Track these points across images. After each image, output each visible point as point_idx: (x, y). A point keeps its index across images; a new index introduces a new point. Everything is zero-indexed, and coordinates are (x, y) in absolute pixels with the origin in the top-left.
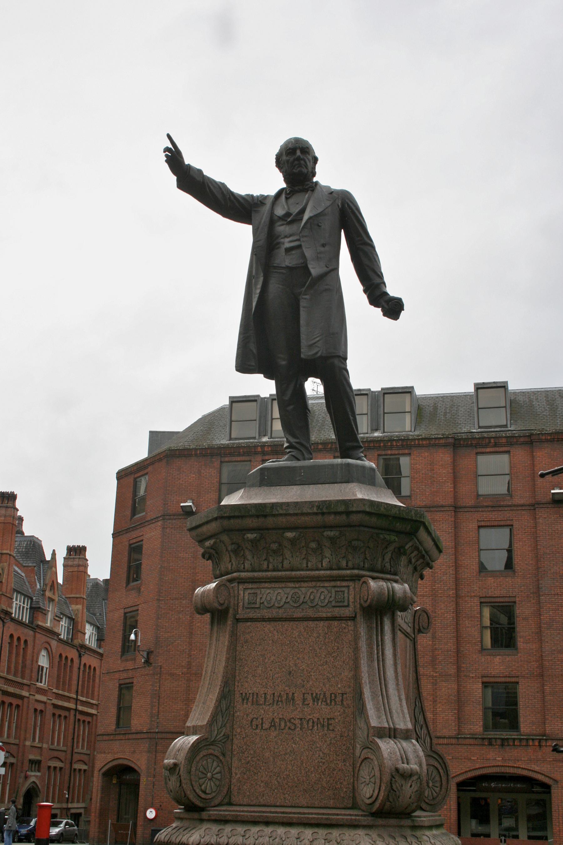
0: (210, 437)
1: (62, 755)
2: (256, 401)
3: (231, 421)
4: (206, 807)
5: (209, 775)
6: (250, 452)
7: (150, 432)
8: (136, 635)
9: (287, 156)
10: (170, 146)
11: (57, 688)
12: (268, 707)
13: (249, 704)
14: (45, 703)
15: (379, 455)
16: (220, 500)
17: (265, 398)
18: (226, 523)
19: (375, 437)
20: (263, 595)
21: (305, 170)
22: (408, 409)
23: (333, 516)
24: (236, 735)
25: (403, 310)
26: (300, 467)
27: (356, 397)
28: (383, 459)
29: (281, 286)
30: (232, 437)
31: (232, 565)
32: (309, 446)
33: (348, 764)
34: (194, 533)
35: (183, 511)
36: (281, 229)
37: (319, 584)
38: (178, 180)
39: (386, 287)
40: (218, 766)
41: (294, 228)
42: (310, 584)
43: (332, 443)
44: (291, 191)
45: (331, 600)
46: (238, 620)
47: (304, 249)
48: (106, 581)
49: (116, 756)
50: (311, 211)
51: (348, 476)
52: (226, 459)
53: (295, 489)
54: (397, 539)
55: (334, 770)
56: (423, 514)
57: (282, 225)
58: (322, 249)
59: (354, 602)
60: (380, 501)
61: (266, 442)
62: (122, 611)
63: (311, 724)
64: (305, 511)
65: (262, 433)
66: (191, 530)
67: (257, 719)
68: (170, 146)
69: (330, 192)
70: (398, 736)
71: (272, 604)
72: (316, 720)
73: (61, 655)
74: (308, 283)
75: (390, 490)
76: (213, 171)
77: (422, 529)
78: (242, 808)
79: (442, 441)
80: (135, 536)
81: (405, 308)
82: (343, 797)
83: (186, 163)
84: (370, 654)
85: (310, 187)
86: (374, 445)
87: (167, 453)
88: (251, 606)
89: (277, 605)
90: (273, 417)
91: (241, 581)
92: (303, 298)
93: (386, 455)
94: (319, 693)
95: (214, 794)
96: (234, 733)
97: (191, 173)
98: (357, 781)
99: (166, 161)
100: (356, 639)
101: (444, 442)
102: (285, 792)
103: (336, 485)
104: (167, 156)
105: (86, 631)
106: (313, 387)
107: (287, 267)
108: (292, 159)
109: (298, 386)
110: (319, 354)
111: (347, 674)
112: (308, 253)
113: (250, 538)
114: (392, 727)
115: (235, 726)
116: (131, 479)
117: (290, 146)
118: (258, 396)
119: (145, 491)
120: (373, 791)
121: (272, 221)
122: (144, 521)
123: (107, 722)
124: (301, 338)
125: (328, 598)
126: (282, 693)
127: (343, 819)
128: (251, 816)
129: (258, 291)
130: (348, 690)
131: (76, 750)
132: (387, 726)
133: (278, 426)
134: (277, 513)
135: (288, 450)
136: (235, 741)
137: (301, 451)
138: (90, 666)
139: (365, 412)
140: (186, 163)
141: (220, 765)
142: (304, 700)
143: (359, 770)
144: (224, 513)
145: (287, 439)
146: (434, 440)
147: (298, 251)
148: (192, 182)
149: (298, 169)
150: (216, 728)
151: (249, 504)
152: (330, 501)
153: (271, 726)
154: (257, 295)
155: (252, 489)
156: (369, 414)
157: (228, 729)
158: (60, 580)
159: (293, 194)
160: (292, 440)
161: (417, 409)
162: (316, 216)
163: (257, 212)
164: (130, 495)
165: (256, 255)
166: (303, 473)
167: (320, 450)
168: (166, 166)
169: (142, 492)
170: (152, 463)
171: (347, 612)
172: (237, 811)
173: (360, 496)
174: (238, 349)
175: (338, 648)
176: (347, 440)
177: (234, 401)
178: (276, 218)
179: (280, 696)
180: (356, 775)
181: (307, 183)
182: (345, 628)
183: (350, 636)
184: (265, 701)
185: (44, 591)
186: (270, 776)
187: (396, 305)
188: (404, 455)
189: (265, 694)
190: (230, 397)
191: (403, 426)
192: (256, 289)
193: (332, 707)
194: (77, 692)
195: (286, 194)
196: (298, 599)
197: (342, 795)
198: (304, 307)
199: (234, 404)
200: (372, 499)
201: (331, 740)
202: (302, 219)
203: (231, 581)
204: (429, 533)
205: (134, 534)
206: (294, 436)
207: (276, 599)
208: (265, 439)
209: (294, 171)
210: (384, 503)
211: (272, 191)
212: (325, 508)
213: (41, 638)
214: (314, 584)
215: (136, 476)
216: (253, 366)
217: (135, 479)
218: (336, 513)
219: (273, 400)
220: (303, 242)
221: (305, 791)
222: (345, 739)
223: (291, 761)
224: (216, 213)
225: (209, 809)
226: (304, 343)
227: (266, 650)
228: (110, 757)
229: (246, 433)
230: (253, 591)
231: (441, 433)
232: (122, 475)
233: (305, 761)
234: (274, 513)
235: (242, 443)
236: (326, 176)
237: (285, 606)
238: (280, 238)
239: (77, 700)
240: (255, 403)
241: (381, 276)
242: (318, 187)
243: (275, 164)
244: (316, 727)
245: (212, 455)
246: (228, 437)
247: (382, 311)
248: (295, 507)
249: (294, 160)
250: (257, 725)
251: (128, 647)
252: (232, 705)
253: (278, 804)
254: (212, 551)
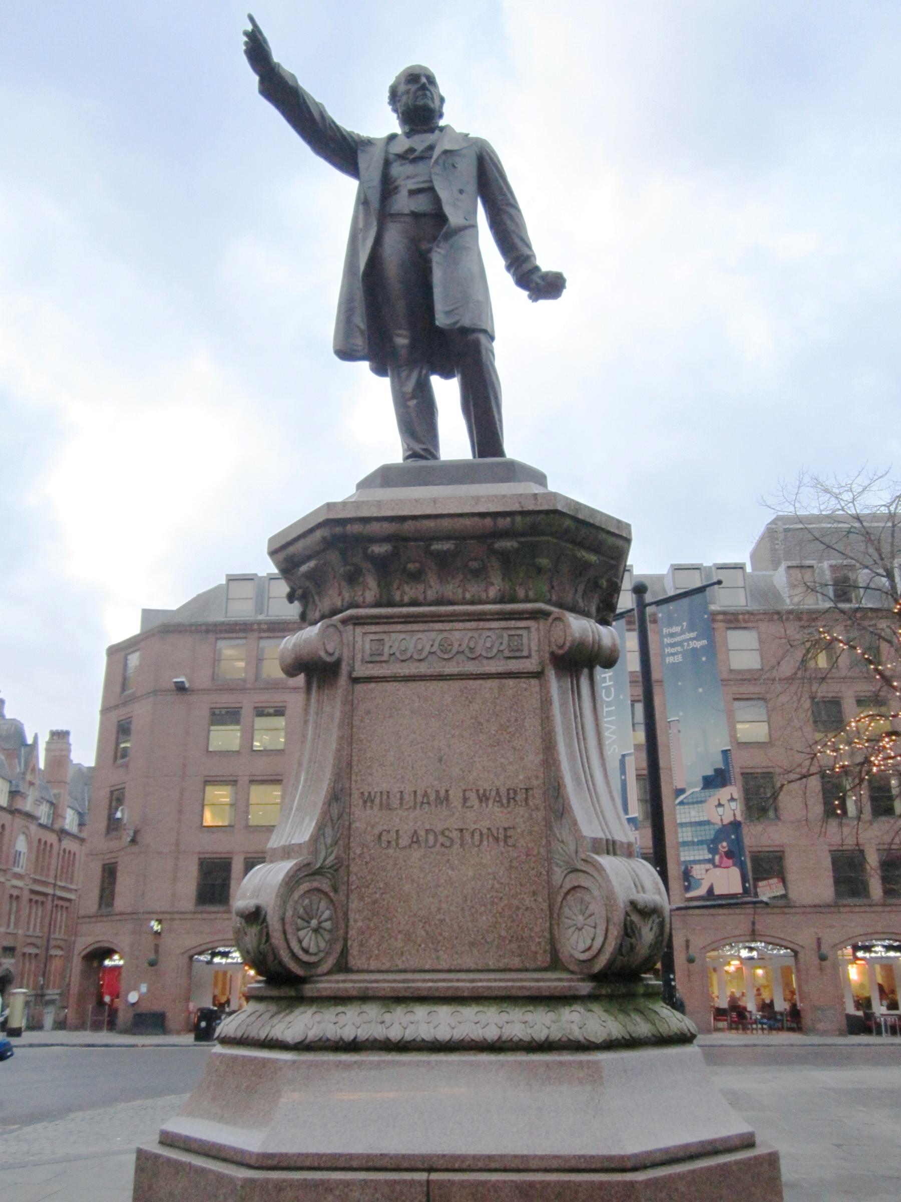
1: (38, 942)
4: (312, 976)
5: (314, 923)
8: (122, 811)
11: (35, 873)
12: (406, 813)
13: (376, 809)
14: (21, 888)
20: (394, 642)
24: (354, 859)
31: (343, 600)
33: (540, 900)
36: (397, 170)
37: (482, 624)
38: (262, 82)
40: (327, 909)
42: (469, 625)
45: (501, 648)
46: (355, 680)
48: (90, 768)
49: (98, 939)
52: (222, 636)
55: (518, 908)
59: (539, 651)
62: (108, 790)
63: (477, 837)
67: (389, 832)
70: (618, 852)
71: (409, 655)
72: (485, 831)
73: (40, 840)
78: (373, 977)
82: (536, 953)
84: (567, 728)
88: (374, 659)
89: (416, 657)
91: (357, 621)
94: (488, 789)
95: (322, 955)
96: (352, 855)
98: (558, 924)
100: (546, 702)
102: (439, 948)
105: (67, 816)
111: (533, 759)
112: (443, 194)
114: (610, 838)
115: (352, 845)
118: (256, 575)
120: (593, 940)
121: (387, 164)
123: (90, 902)
125: (497, 645)
126: (429, 790)
127: (549, 987)
128: (393, 987)
130: (535, 783)
131: (52, 936)
132: (603, 837)
136: (353, 868)
138: (70, 852)
141: (331, 907)
142: (465, 799)
143: (561, 907)
150: (323, 847)
153: (413, 842)
157: (342, 849)
158: (42, 765)
170: (145, 639)
171: (530, 665)
172: (365, 981)
175: (516, 720)
178: (391, 157)
179: (426, 794)
180: (555, 916)
182: (526, 690)
183: (534, 701)
184: (401, 804)
185: (24, 774)
186: (413, 923)
189: (401, 792)
190: (227, 575)
193: (510, 809)
194: (56, 877)
196: (449, 648)
197: (533, 948)
199: (232, 583)
201: (511, 861)
202: (431, 158)
203: (344, 622)
207: (415, 647)
213: (19, 821)
214: (473, 624)
221: (472, 944)
222: (534, 859)
223: (447, 897)
225: (315, 978)
226: (439, 307)
227: (401, 725)
228: (90, 940)
229: (242, 609)
230: (377, 637)
232: (113, 651)
233: (469, 897)
236: (458, 117)
237: (430, 658)
239: (55, 885)
240: (250, 583)
244: (485, 843)
245: (207, 631)
250: (389, 842)
251: (113, 825)
252: (348, 810)
253: (427, 967)
254: (308, 583)
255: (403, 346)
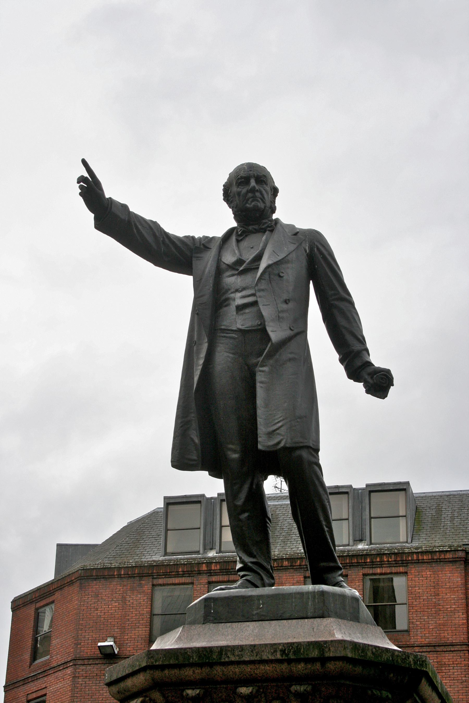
0: (138, 552)
2: (199, 502)
3: (167, 530)
6: (190, 571)
7: (58, 545)
9: (238, 187)
10: (86, 175)
15: (364, 575)
16: (151, 642)
17: (212, 498)
18: (158, 674)
19: (359, 550)
21: (261, 205)
22: (402, 513)
23: (302, 665)
25: (393, 385)
26: (258, 596)
27: (331, 497)
28: (371, 579)
29: (231, 355)
30: (169, 550)
32: (269, 567)
34: (115, 689)
35: (101, 654)
36: (231, 280)
38: (96, 219)
39: (369, 355)
41: (248, 279)
43: (301, 558)
44: (243, 232)
47: (261, 307)
50: (269, 258)
51: (322, 609)
52: (160, 581)
53: (251, 627)
54: (390, 696)
56: (425, 661)
57: (233, 275)
58: (285, 306)
60: (366, 642)
61: (214, 558)
64: (265, 657)
65: (209, 546)
66: (109, 684)
68: (86, 175)
69: (294, 233)
74: (266, 351)
75: (380, 628)
76: (142, 205)
77: (424, 681)
79: (449, 556)
80: (35, 689)
81: (394, 383)
83: (107, 196)
85: (268, 227)
86: (358, 560)
87: (79, 572)
90: (223, 524)
92: (260, 371)
93: (375, 574)
97: (114, 209)
99: (80, 194)
101: (451, 556)
103: (306, 620)
104: (81, 187)
106: (274, 486)
107: (240, 330)
108: (244, 191)
109: (254, 487)
110: (282, 445)
112: (266, 312)
113: (190, 695)
116: (31, 610)
117: (242, 174)
118: (203, 496)
119: (50, 626)
121: (219, 271)
122: (48, 668)
124: (258, 423)
129: (201, 362)
133: (228, 536)
134: (227, 660)
135: (242, 573)
137: (259, 574)
139: (345, 516)
140: (107, 196)
144: (156, 661)
145: (240, 558)
146: (438, 554)
147: (254, 309)
148: (113, 220)
149: (253, 203)
151: (189, 648)
152: (299, 644)
154: (200, 367)
155: (193, 627)
156: (350, 519)
159: (246, 236)
160: (247, 559)
161: (414, 512)
162: (277, 263)
163: (199, 258)
164: (29, 632)
165: (198, 314)
166: (263, 604)
167: (286, 569)
168: (81, 200)
169: (46, 627)
170: (61, 588)
173: (339, 636)
174: (174, 438)
176: (321, 560)
177: (170, 502)
178: (224, 266)
181: (264, 221)
187: (382, 379)
188: (397, 574)
190: (165, 498)
191: (396, 535)
192: (198, 359)
195: (238, 235)
198: (262, 382)
199: (171, 507)
200: (356, 640)
202: (258, 268)
204: (435, 688)
205: (33, 687)
206: (250, 555)
208: (212, 554)
209: (248, 205)
210: (372, 646)
211: (218, 232)
212: (292, 653)
215: (38, 605)
216: (194, 460)
217: (37, 609)
218: (308, 660)
219: (222, 501)
220: (260, 297)
224: (145, 261)
226: (262, 429)
229: (186, 545)
231: (447, 544)
232: (19, 605)
234: (223, 660)
235: (181, 559)
236: (289, 211)
238: (230, 292)
241: (362, 341)
242: (278, 226)
243: (206, 235)
245: (141, 576)
246: (162, 552)
247: (365, 386)
248: (252, 651)
249: (248, 192)
255: (233, 460)
